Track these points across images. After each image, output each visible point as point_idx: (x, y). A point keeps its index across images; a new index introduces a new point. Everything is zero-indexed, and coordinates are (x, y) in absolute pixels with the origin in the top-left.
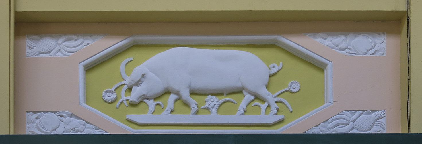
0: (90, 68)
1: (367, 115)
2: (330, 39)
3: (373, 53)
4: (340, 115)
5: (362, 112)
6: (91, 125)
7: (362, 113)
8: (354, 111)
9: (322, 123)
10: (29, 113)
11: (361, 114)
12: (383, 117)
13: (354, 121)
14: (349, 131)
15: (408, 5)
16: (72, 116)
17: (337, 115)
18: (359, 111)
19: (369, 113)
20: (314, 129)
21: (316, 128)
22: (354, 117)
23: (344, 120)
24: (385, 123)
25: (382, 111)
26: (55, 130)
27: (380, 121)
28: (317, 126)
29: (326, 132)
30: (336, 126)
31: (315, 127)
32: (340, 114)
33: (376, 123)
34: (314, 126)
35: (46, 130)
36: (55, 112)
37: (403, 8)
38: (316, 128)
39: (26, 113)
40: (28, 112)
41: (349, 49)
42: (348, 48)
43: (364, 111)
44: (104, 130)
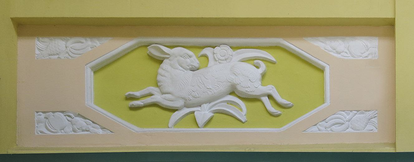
0: (97, 70)
1: (361, 115)
2: (328, 42)
3: (367, 55)
4: (336, 115)
5: (357, 112)
6: (96, 125)
7: (357, 113)
8: (350, 111)
9: (320, 122)
10: (39, 113)
11: (355, 114)
12: (375, 117)
13: (349, 121)
14: (206, 102)
15: (395, 17)
16: (79, 115)
17: (333, 115)
18: (353, 111)
19: (363, 113)
20: (312, 128)
21: (314, 127)
22: (348, 117)
23: (340, 120)
24: (376, 122)
25: (374, 111)
26: (63, 129)
27: (373, 120)
28: (316, 125)
29: (287, 102)
30: (334, 125)
31: (313, 127)
32: (336, 114)
33: (369, 122)
34: (313, 125)
35: (52, 129)
36: (62, 112)
37: (393, 17)
38: (314, 127)
39: (35, 112)
40: (37, 112)
41: (345, 52)
42: (344, 51)
43: (358, 111)
44: (108, 130)
